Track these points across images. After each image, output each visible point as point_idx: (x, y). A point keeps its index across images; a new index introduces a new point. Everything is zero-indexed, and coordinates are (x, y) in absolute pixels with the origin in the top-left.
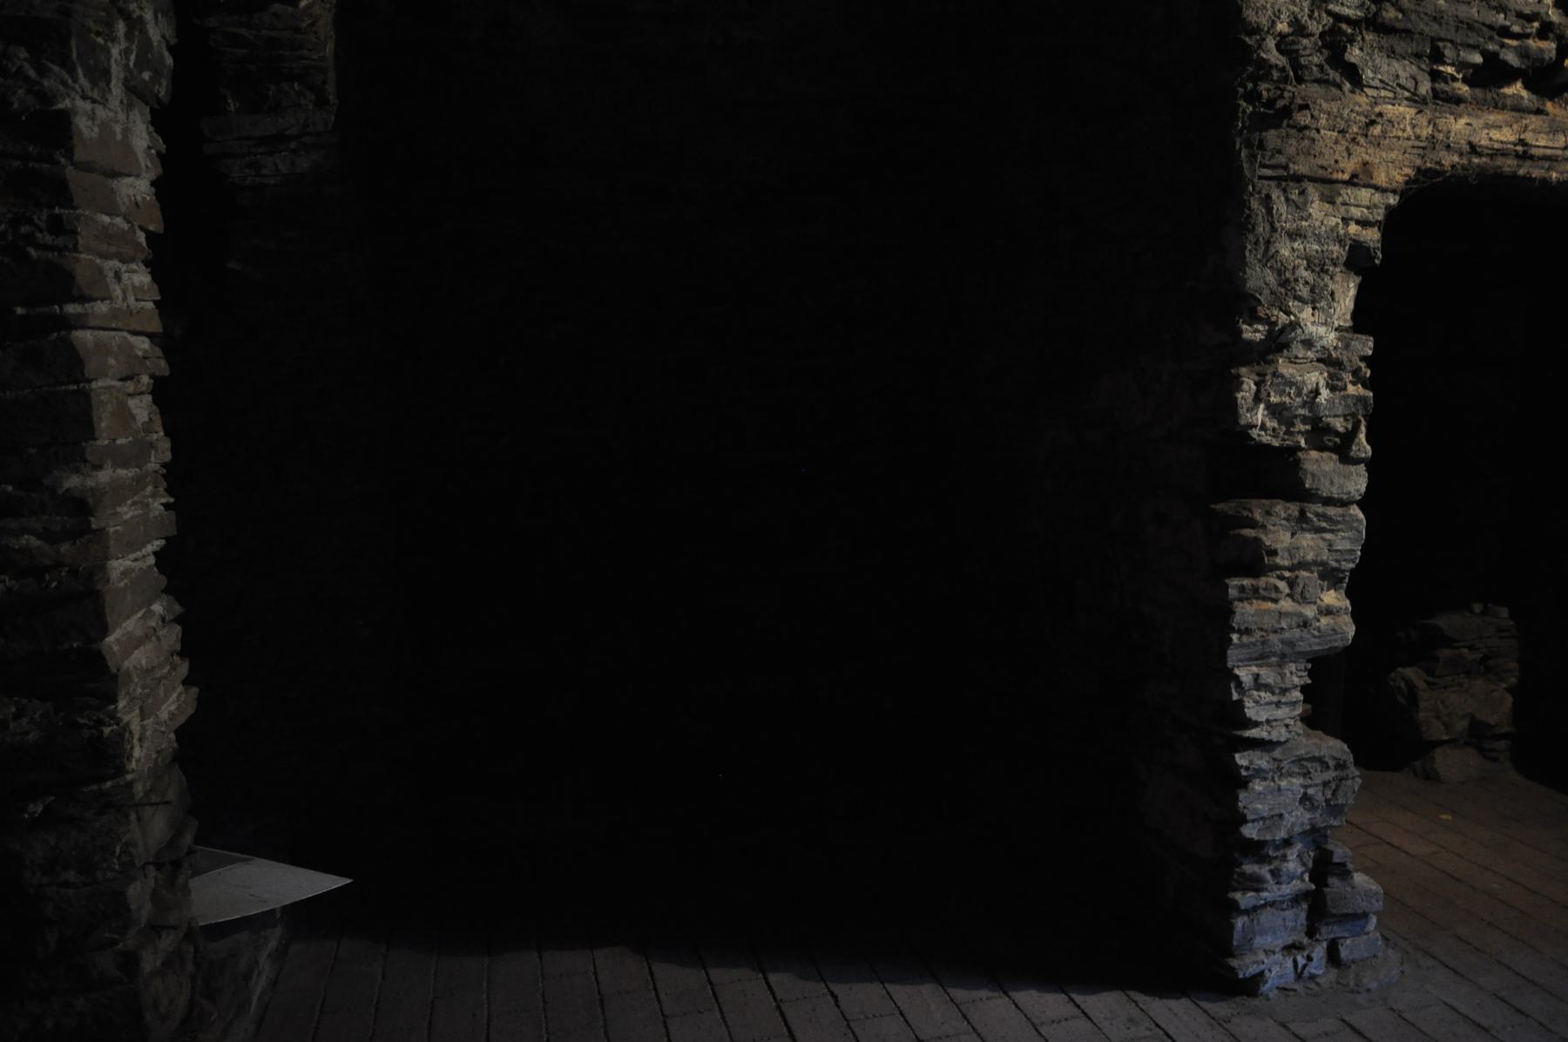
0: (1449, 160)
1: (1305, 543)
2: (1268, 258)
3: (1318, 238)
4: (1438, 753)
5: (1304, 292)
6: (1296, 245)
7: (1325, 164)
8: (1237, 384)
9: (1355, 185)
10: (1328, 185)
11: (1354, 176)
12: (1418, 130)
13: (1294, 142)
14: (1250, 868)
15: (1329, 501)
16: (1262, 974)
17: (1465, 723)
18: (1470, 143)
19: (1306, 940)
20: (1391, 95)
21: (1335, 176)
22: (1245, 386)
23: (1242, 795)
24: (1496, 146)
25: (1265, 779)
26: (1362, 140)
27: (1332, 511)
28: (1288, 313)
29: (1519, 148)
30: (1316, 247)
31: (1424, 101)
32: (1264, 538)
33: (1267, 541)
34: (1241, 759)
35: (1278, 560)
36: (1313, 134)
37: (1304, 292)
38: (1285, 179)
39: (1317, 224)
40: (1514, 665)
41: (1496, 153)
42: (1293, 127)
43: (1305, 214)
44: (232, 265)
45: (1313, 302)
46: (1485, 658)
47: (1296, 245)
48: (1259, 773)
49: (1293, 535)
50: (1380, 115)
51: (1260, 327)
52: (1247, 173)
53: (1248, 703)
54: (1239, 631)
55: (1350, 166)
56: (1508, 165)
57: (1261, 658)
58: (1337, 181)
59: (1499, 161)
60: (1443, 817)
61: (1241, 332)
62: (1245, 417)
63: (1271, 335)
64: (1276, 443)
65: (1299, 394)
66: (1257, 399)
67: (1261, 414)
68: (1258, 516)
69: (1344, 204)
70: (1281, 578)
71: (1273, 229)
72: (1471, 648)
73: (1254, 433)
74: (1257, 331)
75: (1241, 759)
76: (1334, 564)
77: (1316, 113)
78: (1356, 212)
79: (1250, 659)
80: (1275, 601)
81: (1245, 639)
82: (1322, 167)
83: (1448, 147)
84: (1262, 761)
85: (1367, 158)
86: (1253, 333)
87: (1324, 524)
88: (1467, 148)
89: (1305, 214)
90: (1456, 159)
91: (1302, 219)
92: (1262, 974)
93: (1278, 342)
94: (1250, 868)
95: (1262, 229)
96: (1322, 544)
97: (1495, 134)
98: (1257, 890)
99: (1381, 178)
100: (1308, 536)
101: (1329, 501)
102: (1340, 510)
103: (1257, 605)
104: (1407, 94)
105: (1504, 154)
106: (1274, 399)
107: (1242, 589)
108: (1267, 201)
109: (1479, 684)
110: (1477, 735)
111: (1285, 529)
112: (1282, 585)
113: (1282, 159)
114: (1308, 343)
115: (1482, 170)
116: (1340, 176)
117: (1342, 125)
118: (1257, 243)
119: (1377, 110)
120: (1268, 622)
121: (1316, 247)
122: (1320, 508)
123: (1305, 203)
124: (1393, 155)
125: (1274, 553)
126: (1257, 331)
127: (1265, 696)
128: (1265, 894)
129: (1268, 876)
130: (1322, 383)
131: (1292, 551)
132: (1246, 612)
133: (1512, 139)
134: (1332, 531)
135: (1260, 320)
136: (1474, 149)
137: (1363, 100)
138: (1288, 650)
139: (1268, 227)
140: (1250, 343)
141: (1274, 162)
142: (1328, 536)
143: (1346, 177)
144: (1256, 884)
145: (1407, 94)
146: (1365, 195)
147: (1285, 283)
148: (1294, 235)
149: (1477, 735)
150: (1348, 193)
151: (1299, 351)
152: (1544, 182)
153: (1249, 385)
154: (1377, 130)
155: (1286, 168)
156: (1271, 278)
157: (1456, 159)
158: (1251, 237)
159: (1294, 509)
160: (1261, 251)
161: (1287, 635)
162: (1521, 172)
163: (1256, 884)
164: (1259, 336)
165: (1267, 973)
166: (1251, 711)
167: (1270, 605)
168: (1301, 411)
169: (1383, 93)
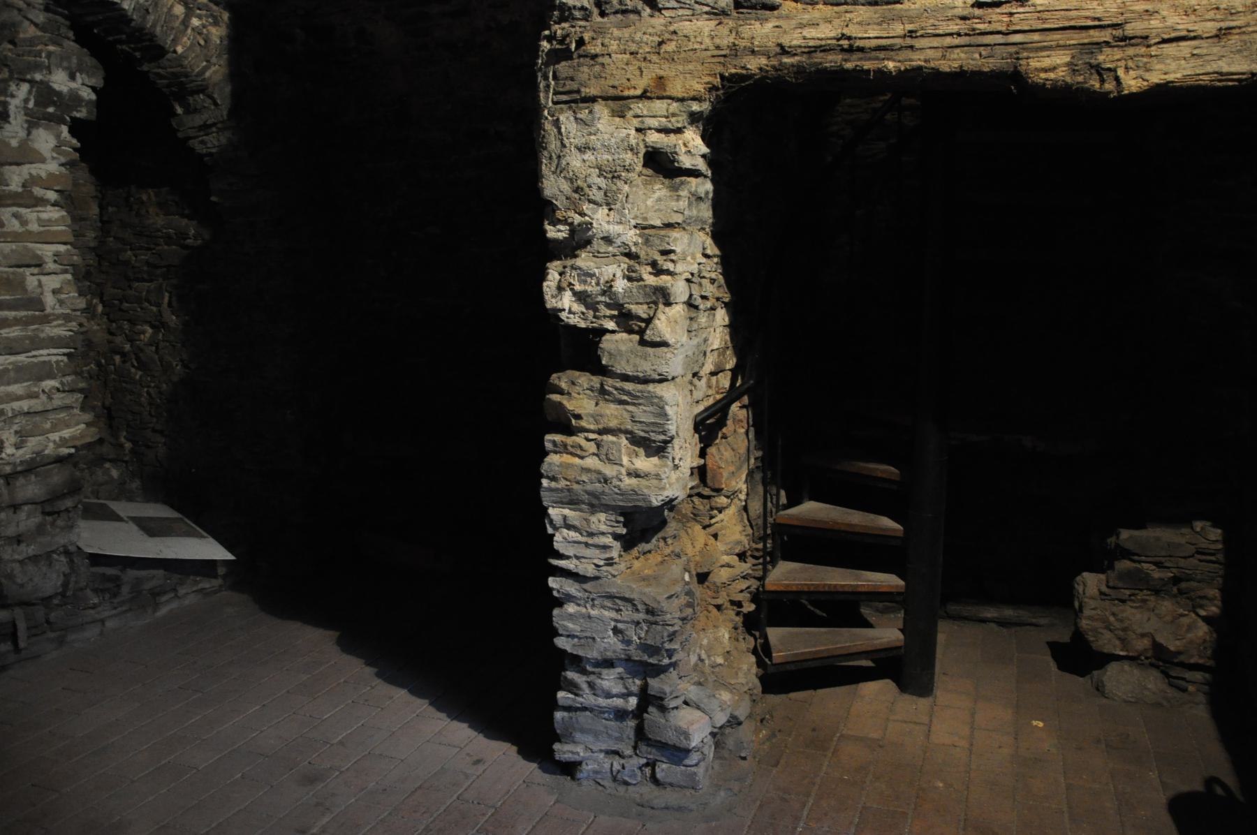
0: (754, 64)
1: (608, 412)
2: (559, 170)
3: (608, 148)
4: (1113, 668)
5: (598, 196)
6: (586, 157)
7: (616, 83)
8: (543, 276)
9: (650, 98)
10: (619, 102)
11: (645, 91)
12: (717, 41)
13: (585, 69)
14: (570, 675)
15: (625, 378)
16: (580, 763)
17: (1146, 643)
18: (780, 45)
19: (629, 752)
20: (689, 12)
21: (626, 93)
22: (550, 277)
23: (556, 612)
24: (811, 43)
25: (579, 605)
26: (655, 58)
27: (629, 386)
28: (582, 214)
29: (845, 43)
30: (606, 157)
31: (724, 13)
32: (565, 402)
33: (569, 405)
34: (553, 582)
35: (583, 424)
36: (606, 60)
37: (598, 196)
38: (575, 101)
39: (606, 137)
40: (1214, 592)
41: (811, 51)
42: (586, 56)
43: (592, 130)
44: (213, 199)
45: (608, 204)
46: (1176, 580)
47: (586, 157)
48: (570, 598)
49: (597, 404)
50: (675, 32)
51: (561, 227)
52: (543, 101)
53: (558, 538)
54: (548, 477)
55: (641, 84)
56: (831, 61)
57: (573, 502)
58: (628, 98)
59: (818, 57)
60: (1035, 723)
61: (545, 232)
62: (551, 303)
63: (573, 231)
64: (583, 325)
65: (598, 284)
66: (560, 289)
67: (567, 300)
68: (563, 385)
69: (636, 116)
70: (588, 440)
71: (564, 146)
72: (1158, 565)
73: (563, 315)
74: (559, 231)
75: (553, 582)
76: (642, 434)
77: (606, 41)
78: (654, 123)
79: (562, 503)
80: (582, 458)
81: (553, 484)
82: (613, 87)
83: (753, 52)
84: (570, 587)
85: (662, 73)
86: (555, 232)
87: (625, 398)
88: (778, 49)
89: (592, 130)
90: (763, 61)
91: (590, 134)
92: (580, 763)
93: (579, 240)
94: (570, 675)
95: (553, 145)
96: (626, 415)
97: (810, 33)
98: (576, 695)
99: (676, 89)
100: (612, 406)
101: (625, 378)
102: (640, 387)
103: (567, 458)
104: (706, 9)
105: (825, 49)
106: (578, 288)
107: (554, 443)
108: (557, 123)
109: (1166, 606)
110: (1161, 659)
111: (590, 398)
112: (592, 447)
113: (575, 86)
114: (608, 240)
115: (799, 70)
116: (632, 93)
117: (634, 48)
118: (551, 158)
119: (671, 28)
120: (572, 474)
121: (606, 157)
122: (619, 384)
123: (593, 119)
124: (691, 67)
125: (578, 417)
126: (559, 231)
127: (573, 535)
128: (580, 699)
129: (585, 686)
130: (619, 274)
131: (596, 417)
132: (553, 460)
133: (833, 34)
134: (634, 404)
135: (559, 222)
136: (784, 51)
137: (662, 21)
138: (595, 502)
139: (559, 144)
140: (555, 241)
141: (567, 88)
142: (630, 408)
143: (638, 92)
144: (573, 687)
145: (706, 9)
146: (660, 106)
147: (577, 190)
148: (582, 149)
149: (1161, 659)
150: (639, 107)
151: (597, 245)
152: (881, 73)
153: (553, 276)
154: (670, 47)
155: (578, 92)
156: (566, 187)
157: (763, 61)
158: (545, 153)
159: (596, 381)
160: (554, 165)
161: (589, 487)
162: (849, 66)
163: (573, 687)
164: (561, 236)
165: (584, 766)
166: (559, 543)
167: (577, 461)
168: (603, 299)
169: (681, 12)
